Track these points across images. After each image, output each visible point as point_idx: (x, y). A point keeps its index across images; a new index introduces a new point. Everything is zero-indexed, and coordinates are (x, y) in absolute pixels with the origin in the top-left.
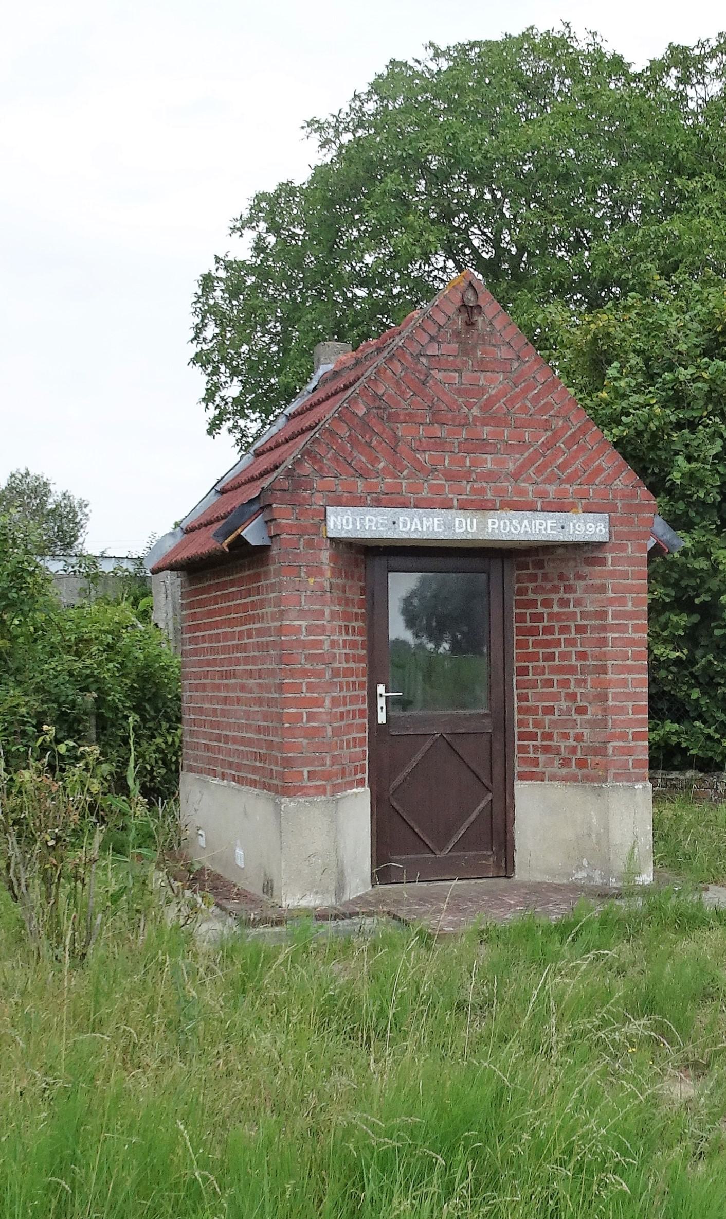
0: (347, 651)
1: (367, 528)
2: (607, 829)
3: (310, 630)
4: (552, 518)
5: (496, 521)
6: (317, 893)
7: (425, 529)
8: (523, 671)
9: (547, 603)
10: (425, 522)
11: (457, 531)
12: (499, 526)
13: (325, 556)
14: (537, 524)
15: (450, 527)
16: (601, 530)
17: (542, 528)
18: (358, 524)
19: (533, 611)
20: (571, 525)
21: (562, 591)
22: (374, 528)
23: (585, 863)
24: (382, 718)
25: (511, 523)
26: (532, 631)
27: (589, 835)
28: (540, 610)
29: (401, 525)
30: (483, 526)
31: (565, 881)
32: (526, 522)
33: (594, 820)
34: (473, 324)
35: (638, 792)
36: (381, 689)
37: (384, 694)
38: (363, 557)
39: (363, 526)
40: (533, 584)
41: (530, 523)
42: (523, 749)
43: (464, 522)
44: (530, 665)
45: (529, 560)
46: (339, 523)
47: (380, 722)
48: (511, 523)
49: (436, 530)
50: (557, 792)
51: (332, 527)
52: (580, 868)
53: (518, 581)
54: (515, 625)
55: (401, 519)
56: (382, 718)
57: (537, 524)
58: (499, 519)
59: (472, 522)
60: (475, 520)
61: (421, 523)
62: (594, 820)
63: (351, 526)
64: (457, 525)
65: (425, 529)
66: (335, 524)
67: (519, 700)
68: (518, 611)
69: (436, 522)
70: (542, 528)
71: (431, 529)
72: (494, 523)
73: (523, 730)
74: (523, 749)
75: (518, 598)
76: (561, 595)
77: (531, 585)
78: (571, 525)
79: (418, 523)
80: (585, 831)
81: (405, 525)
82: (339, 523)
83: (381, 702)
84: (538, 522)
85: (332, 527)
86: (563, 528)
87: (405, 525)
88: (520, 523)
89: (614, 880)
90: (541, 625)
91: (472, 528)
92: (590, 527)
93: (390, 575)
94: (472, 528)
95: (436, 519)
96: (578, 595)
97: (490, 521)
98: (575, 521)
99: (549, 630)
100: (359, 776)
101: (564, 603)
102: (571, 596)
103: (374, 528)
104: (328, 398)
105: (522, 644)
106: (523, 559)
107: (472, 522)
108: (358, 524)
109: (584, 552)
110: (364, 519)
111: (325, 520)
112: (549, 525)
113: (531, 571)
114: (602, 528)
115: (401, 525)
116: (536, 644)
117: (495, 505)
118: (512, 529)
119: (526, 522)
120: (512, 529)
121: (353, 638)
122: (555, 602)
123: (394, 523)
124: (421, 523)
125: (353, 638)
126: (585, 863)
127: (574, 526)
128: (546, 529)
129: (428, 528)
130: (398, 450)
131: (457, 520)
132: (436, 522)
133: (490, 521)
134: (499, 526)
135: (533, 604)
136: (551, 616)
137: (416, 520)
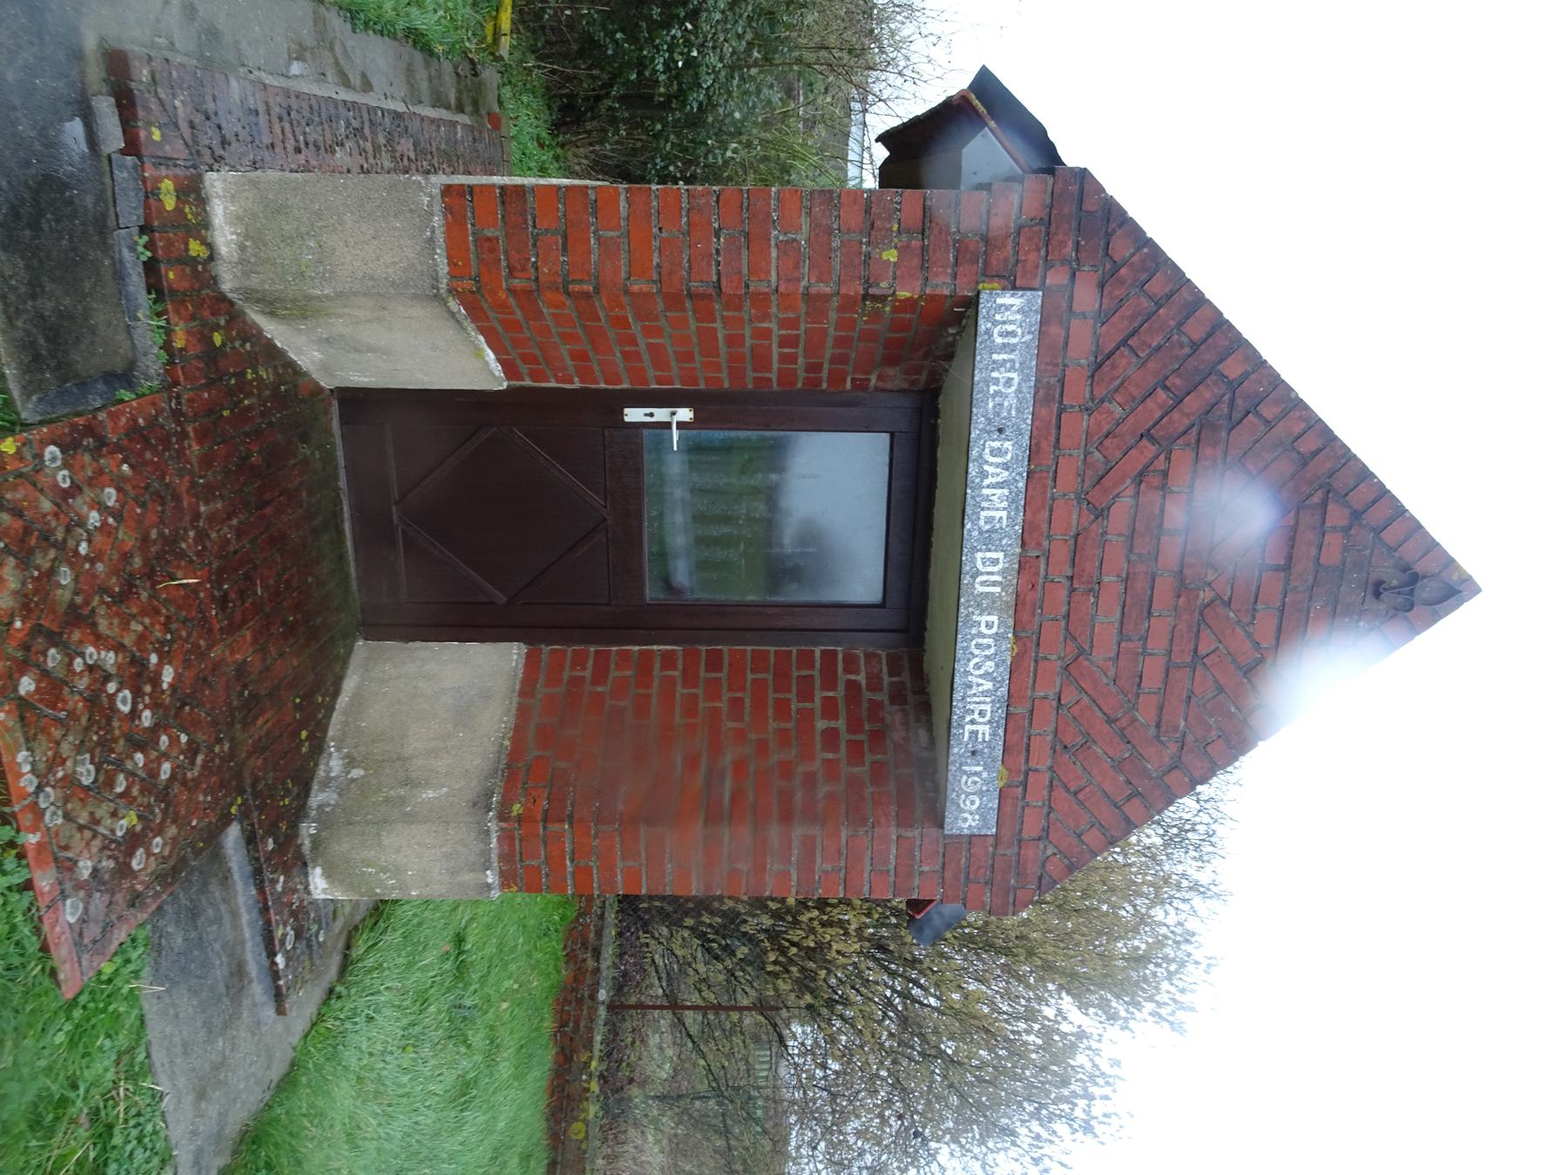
0: (748, 342)
1: (995, 374)
2: (410, 819)
3: (787, 247)
4: (994, 734)
5: (994, 630)
6: (242, 248)
7: (986, 492)
8: (714, 662)
9: (830, 710)
10: (999, 492)
11: (979, 555)
12: (984, 636)
13: (942, 285)
14: (983, 707)
15: (990, 539)
16: (965, 820)
17: (976, 716)
18: (1005, 356)
19: (818, 684)
20: (979, 769)
21: (853, 737)
22: (993, 388)
23: (356, 773)
24: (634, 415)
25: (988, 658)
26: (782, 676)
27: (406, 782)
28: (819, 695)
29: (996, 444)
30: (987, 604)
31: (331, 733)
32: (988, 685)
33: (431, 794)
34: (1377, 595)
35: (481, 876)
36: (685, 414)
37: (676, 419)
38: (921, 386)
39: (998, 365)
40: (864, 683)
41: (985, 693)
42: (579, 661)
43: (995, 569)
44: (723, 675)
45: (905, 676)
46: (1008, 315)
47: (627, 411)
48: (988, 658)
49: (983, 514)
50: (494, 723)
51: (1000, 301)
52: (351, 762)
53: (868, 656)
54: (794, 650)
55: (1008, 445)
56: (634, 415)
57: (983, 707)
58: (996, 637)
59: (994, 584)
60: (998, 589)
61: (1000, 485)
62: (431, 794)
63: (999, 340)
64: (989, 555)
65: (986, 492)
66: (1008, 308)
67: (665, 654)
68: (818, 654)
69: (997, 514)
70: (976, 716)
71: (985, 504)
72: (989, 625)
73: (613, 659)
74: (579, 661)
75: (840, 657)
76: (845, 736)
77: (861, 678)
78: (979, 769)
79: (999, 479)
80: (414, 775)
81: (994, 452)
82: (1008, 315)
83: (661, 414)
84: (988, 708)
85: (1000, 301)
86: (974, 753)
87: (994, 452)
88: (984, 676)
89: (313, 831)
90: (793, 696)
91: (983, 583)
92: (973, 802)
93: (886, 437)
94: (983, 583)
95: (1004, 514)
96: (845, 769)
97: (994, 618)
98: (985, 775)
99: (782, 709)
100: (524, 369)
101: (831, 737)
102: (843, 753)
103: (993, 388)
104: (1059, 428)
105: (759, 660)
106: (906, 664)
107: (994, 584)
108: (1005, 356)
109: (925, 796)
110: (1012, 369)
111: (1014, 288)
112: (980, 728)
113: (886, 679)
114: (970, 822)
115: (996, 444)
116: (760, 685)
117: (1024, 629)
118: (976, 660)
119: (988, 685)
120: (976, 660)
121: (775, 358)
122: (832, 724)
123: (1000, 431)
124: (1000, 485)
125: (775, 358)
126: (356, 773)
127: (976, 774)
128: (973, 722)
129: (987, 498)
130: (1145, 442)
131: (1000, 555)
132: (997, 514)
133: (994, 618)
134: (984, 636)
135: (830, 682)
136: (807, 715)
137: (1006, 474)
